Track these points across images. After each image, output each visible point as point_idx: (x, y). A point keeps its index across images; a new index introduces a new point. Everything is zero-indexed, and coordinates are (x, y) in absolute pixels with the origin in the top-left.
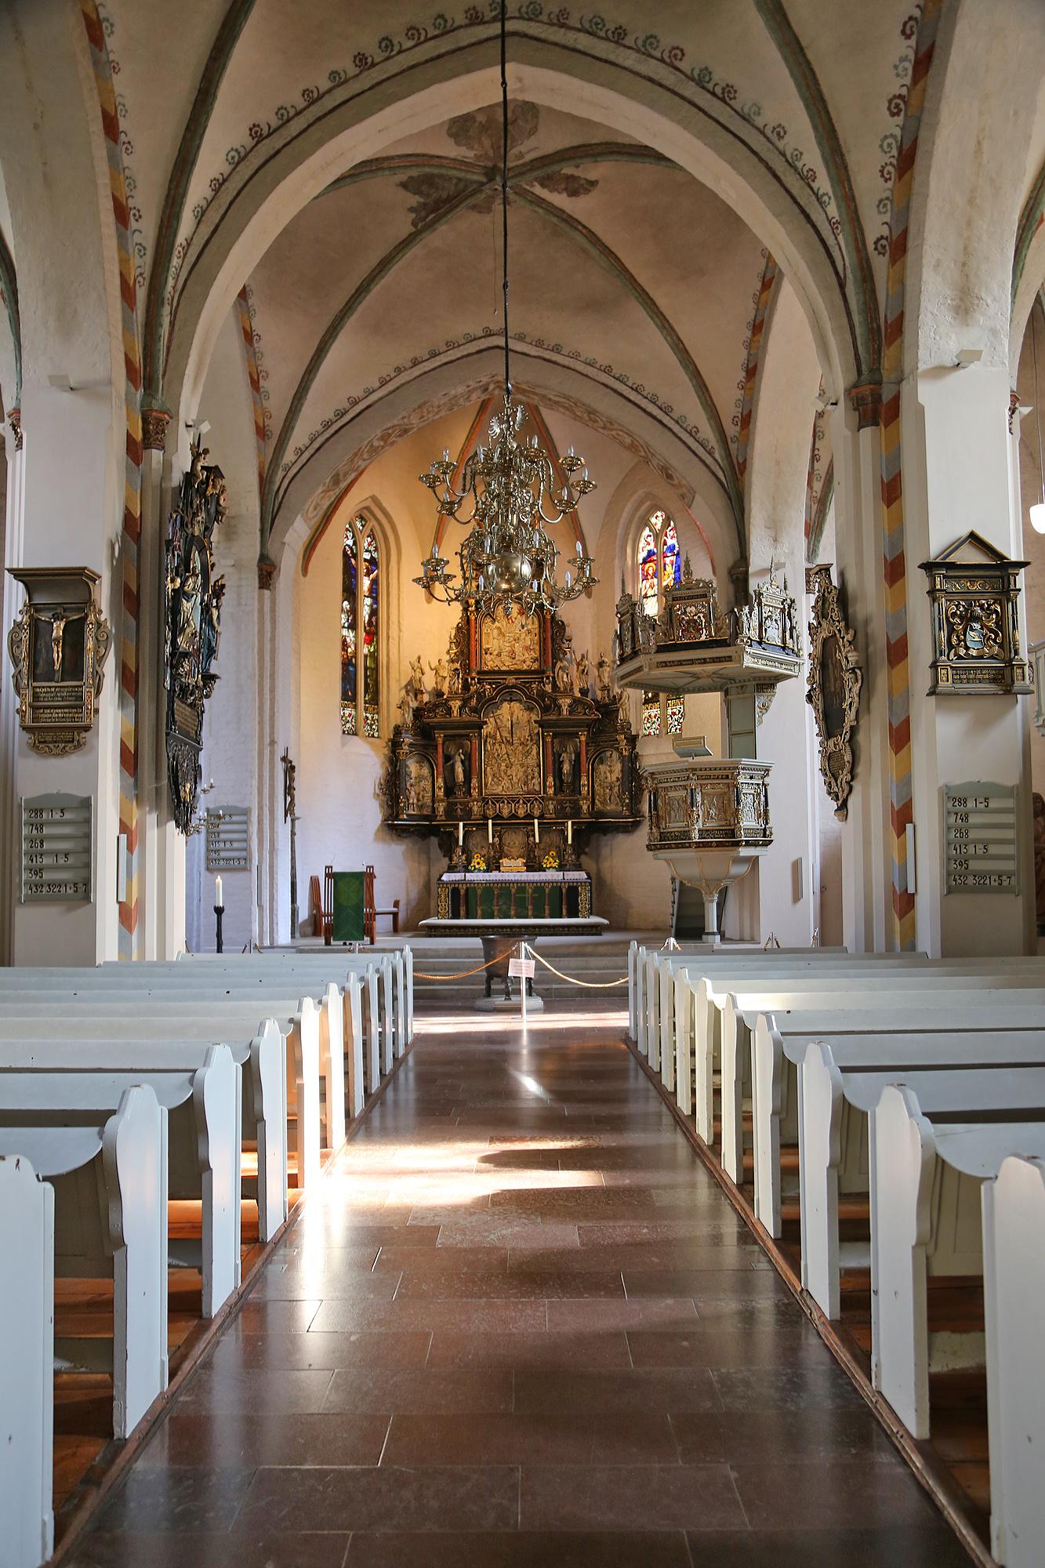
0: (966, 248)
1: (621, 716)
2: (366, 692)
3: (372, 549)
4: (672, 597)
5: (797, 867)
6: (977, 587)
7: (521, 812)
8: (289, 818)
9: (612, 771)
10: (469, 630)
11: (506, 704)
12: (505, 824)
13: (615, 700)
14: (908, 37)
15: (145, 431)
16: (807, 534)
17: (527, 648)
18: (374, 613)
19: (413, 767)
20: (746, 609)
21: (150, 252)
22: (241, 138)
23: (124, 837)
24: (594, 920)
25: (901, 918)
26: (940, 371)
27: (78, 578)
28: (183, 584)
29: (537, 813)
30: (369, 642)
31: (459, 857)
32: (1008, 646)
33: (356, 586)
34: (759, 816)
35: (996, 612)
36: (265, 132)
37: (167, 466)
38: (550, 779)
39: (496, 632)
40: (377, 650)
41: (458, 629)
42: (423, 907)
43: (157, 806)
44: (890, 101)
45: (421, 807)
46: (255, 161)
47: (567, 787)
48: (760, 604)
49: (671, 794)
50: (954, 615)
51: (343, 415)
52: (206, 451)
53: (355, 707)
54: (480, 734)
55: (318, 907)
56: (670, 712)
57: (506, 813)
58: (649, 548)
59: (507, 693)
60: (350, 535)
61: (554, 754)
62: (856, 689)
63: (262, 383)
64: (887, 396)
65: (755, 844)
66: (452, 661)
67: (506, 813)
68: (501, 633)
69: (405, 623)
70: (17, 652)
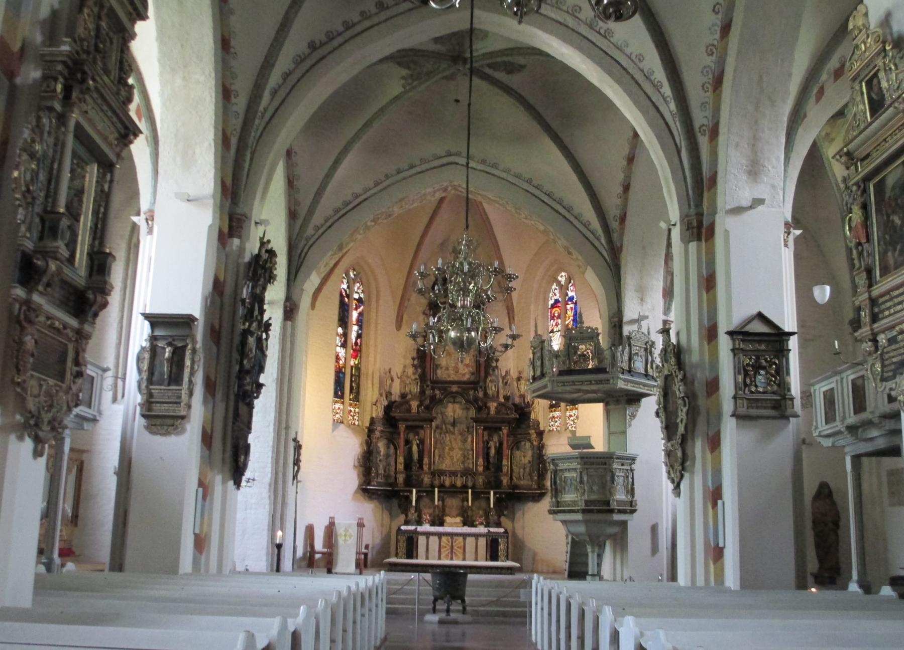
0: (754, 136)
1: (533, 416)
2: (351, 392)
3: (360, 291)
4: (570, 338)
5: (654, 529)
6: (763, 347)
7: (459, 484)
9: (525, 456)
11: (450, 405)
12: (448, 491)
13: (529, 405)
14: (717, 13)
15: (230, 227)
17: (467, 365)
20: (620, 348)
21: (242, 116)
22: (303, 48)
23: (201, 490)
25: (714, 563)
26: (738, 210)
27: (187, 321)
28: (250, 326)
29: (470, 484)
30: (355, 358)
31: (412, 514)
32: (784, 386)
34: (628, 492)
35: (775, 364)
36: (318, 45)
37: (242, 249)
42: (385, 549)
43: (222, 472)
44: (707, 47)
46: (309, 62)
47: (493, 466)
48: (630, 345)
49: (567, 474)
50: (748, 365)
52: (269, 241)
53: (343, 403)
55: (312, 546)
56: (568, 414)
57: (447, 483)
58: (555, 298)
59: (453, 396)
60: (345, 281)
61: (483, 442)
62: (685, 410)
63: (295, 183)
64: (705, 223)
65: (624, 512)
67: (447, 483)
70: (141, 365)
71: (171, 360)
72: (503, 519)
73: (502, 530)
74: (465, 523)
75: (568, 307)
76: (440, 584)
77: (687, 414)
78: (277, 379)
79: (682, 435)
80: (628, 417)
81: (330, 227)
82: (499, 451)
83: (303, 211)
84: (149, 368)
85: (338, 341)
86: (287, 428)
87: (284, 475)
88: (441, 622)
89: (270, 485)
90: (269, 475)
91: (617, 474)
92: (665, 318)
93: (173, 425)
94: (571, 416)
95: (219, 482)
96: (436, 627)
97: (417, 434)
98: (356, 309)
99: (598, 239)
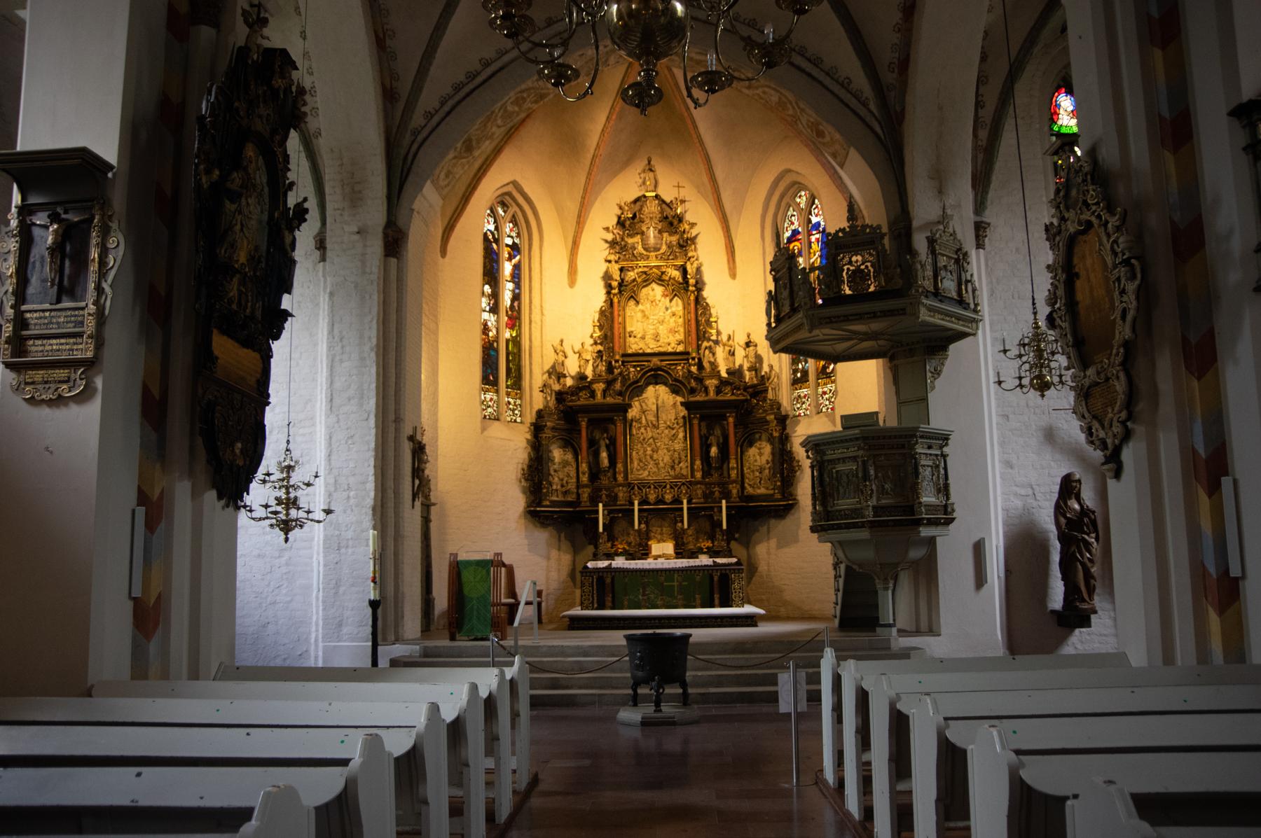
1: (770, 395)
3: (514, 234)
5: (979, 549)
8: (418, 503)
9: (760, 455)
10: (612, 313)
16: (974, 186)
18: (516, 297)
19: (557, 454)
23: (141, 511)
24: (748, 609)
25: (1221, 613)
30: (512, 327)
31: (605, 546)
33: (498, 270)
34: (939, 491)
38: (698, 462)
39: (639, 315)
40: (519, 335)
41: (602, 312)
43: (191, 474)
45: (565, 493)
49: (840, 467)
51: (475, 76)
53: (497, 392)
54: (625, 418)
56: (820, 390)
59: (656, 377)
60: (492, 220)
61: (701, 437)
63: (388, 42)
66: (596, 343)
67: (652, 497)
68: (645, 316)
69: (546, 306)
71: (57, 250)
72: (733, 545)
73: (734, 560)
74: (679, 555)
75: (813, 238)
76: (641, 659)
77: (1137, 298)
78: (378, 345)
79: (1126, 344)
80: (929, 375)
81: (448, 113)
82: (724, 449)
83: (405, 87)
84: (18, 271)
85: (484, 302)
86: (398, 420)
87: (397, 493)
88: (645, 723)
89: (374, 509)
90: (372, 494)
91: (923, 462)
92: (979, 219)
93: (67, 381)
94: (825, 393)
95: (186, 498)
96: (636, 733)
97: (606, 431)
98: (510, 259)
99: (865, 105)
